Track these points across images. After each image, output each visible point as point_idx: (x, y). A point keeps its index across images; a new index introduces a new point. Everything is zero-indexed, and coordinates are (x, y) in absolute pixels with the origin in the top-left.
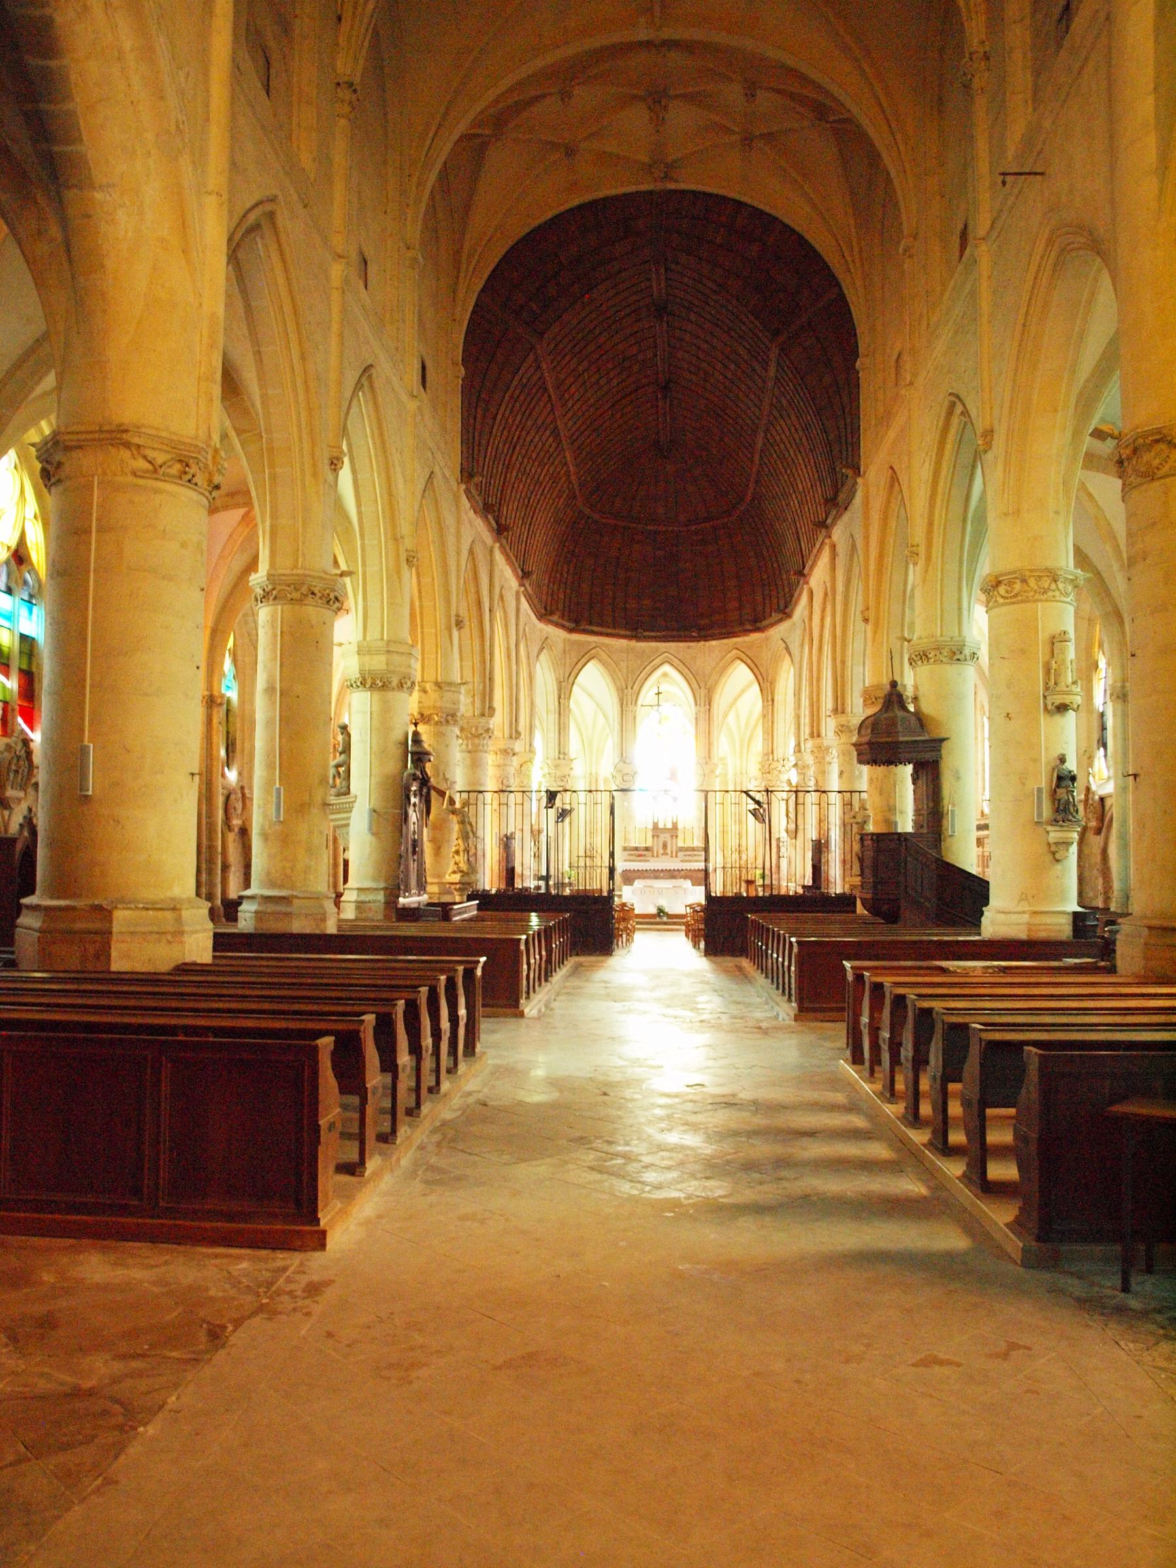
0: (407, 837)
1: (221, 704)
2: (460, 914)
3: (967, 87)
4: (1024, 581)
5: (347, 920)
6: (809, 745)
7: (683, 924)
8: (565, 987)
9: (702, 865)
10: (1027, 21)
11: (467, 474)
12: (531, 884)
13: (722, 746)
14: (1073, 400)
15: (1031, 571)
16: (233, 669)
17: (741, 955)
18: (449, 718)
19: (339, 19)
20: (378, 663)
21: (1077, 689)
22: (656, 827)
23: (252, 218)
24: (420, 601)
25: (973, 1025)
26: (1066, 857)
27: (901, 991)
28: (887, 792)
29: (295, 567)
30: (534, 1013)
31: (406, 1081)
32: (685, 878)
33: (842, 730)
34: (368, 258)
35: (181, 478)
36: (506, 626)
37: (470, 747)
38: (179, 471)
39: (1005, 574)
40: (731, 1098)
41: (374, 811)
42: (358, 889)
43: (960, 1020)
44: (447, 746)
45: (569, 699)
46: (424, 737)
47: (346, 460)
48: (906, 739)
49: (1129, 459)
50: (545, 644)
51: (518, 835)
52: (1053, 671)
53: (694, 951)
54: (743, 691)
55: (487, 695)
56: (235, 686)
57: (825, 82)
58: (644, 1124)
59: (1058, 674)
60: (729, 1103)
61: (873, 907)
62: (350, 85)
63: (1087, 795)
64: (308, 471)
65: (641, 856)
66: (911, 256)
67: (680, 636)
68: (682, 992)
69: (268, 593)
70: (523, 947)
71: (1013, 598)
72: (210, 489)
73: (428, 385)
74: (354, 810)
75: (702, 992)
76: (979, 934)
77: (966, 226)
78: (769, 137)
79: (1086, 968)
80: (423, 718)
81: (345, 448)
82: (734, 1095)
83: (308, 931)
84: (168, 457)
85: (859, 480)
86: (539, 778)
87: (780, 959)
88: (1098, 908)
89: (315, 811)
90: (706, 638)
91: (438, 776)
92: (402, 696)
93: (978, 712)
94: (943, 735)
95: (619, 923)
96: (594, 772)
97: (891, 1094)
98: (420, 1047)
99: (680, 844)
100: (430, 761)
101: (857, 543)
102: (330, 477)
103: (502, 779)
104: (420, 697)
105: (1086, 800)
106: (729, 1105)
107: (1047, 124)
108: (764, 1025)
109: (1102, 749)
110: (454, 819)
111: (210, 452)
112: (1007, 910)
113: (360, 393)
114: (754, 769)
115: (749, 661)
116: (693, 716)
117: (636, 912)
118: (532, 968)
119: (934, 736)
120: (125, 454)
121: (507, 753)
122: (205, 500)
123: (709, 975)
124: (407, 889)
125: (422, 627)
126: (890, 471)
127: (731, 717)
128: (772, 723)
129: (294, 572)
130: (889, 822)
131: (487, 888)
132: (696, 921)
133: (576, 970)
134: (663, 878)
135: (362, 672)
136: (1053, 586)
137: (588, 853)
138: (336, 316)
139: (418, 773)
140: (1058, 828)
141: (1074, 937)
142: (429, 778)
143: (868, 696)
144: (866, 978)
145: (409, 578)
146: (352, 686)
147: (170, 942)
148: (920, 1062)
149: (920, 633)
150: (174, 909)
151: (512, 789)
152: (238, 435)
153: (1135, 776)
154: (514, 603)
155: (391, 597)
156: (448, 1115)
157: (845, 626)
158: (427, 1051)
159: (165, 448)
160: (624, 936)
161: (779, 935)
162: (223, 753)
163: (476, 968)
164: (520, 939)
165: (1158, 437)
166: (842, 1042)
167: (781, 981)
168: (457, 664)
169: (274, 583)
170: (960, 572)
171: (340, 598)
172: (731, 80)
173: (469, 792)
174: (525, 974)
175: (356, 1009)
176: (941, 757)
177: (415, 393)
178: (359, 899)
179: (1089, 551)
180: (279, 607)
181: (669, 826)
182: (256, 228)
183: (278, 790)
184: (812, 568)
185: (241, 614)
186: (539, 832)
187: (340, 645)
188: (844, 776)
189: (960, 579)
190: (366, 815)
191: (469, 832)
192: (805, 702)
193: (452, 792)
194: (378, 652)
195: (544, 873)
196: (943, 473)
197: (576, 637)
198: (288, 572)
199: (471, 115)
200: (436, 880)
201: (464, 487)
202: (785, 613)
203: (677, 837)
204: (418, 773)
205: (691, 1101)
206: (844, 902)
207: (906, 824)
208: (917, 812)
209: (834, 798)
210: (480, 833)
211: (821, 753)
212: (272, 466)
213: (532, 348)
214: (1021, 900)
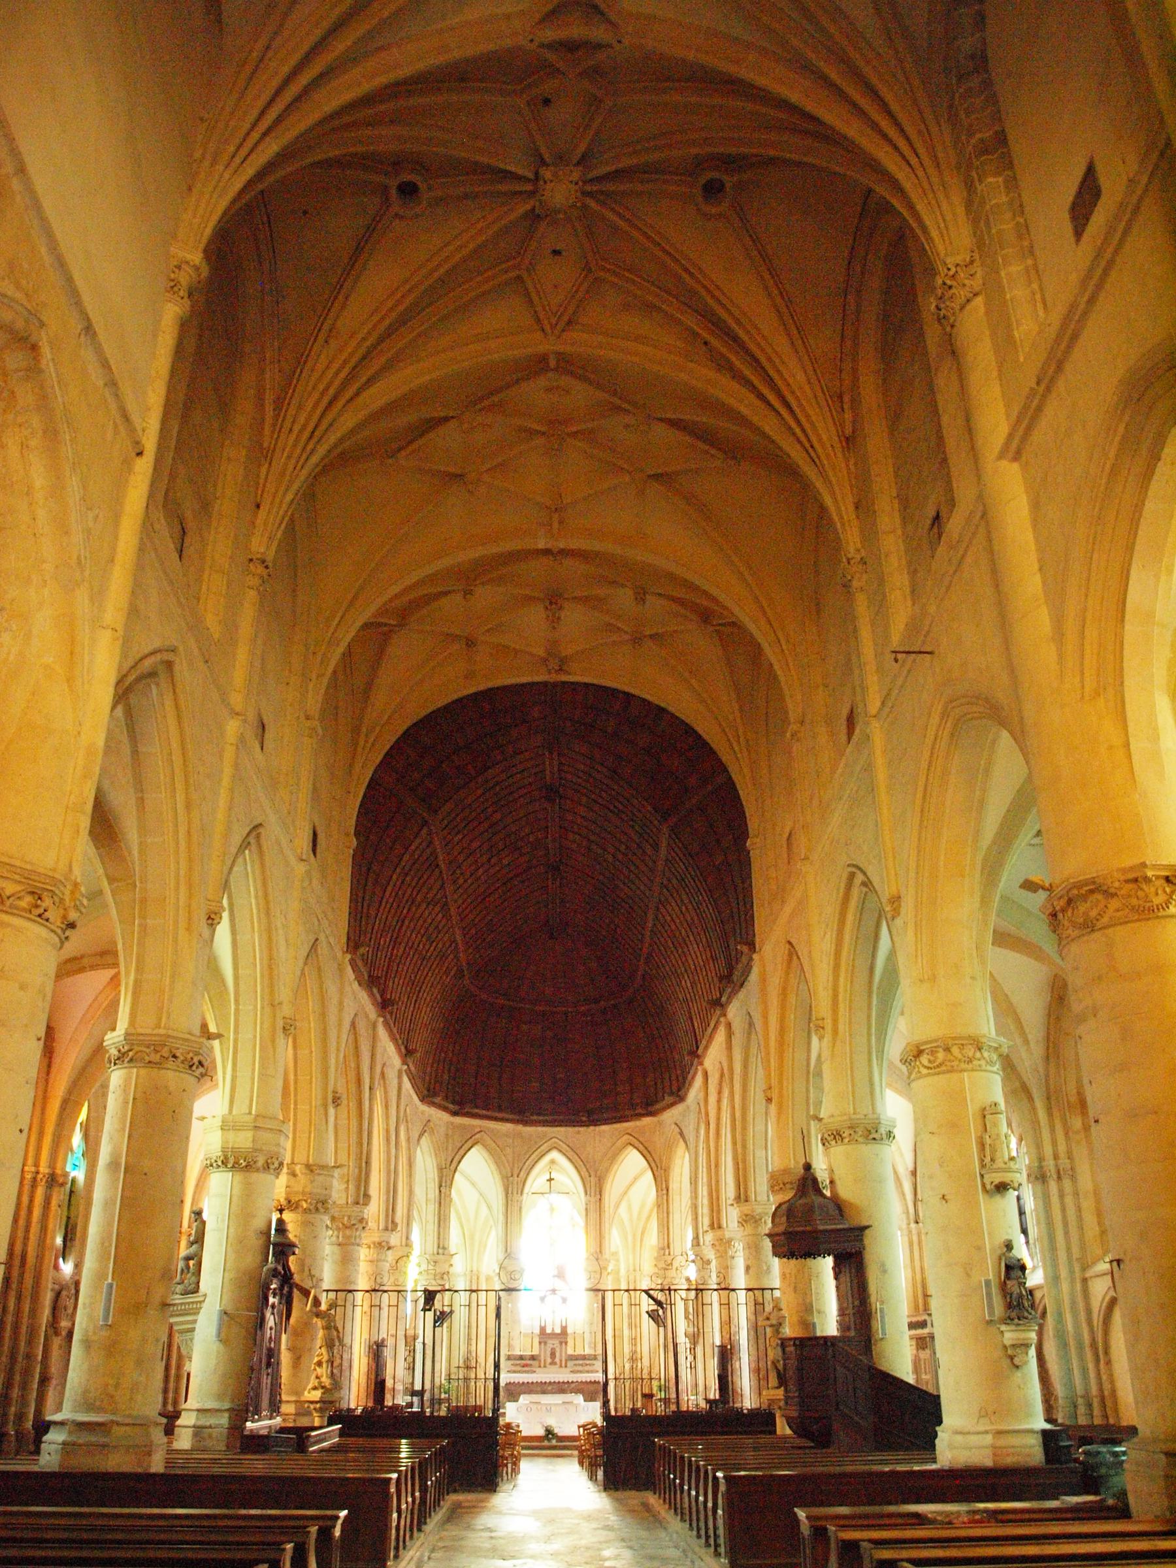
0: (261, 1346)
4: (947, 1049)
6: (709, 1238)
7: (576, 1448)
10: (899, 532)
11: (353, 944)
12: (401, 1400)
13: (615, 1239)
14: (979, 867)
15: (954, 1038)
16: (83, 1145)
18: (320, 1205)
19: (258, 506)
20: (244, 1140)
23: (148, 663)
24: (296, 1075)
26: (1026, 1363)
28: (803, 1290)
29: (158, 1026)
32: (577, 1391)
33: (748, 1219)
34: (265, 721)
36: (387, 1107)
38: (29, 904)
39: (926, 1043)
42: (198, 1410)
46: (290, 1227)
49: (1063, 911)
50: (427, 1127)
51: (390, 1342)
52: (987, 1147)
53: (590, 1484)
54: (635, 1179)
56: (83, 1165)
57: (715, 592)
59: (994, 1150)
61: (800, 1427)
62: (263, 562)
64: (182, 925)
65: (526, 1365)
68: (583, 1542)
69: (124, 1054)
70: (393, 1490)
71: (936, 1068)
72: (64, 926)
73: (318, 851)
76: (934, 1460)
77: (852, 712)
80: (291, 1204)
81: (225, 902)
84: (19, 888)
85: (755, 956)
86: (415, 1276)
87: (701, 1498)
90: (595, 1123)
91: (303, 1271)
94: (865, 1223)
95: (503, 1450)
96: (475, 1269)
99: (570, 1351)
100: (294, 1253)
101: (755, 1021)
102: (206, 932)
103: (376, 1275)
104: (288, 1181)
110: (319, 1323)
112: (966, 1430)
114: (648, 1265)
121: (382, 1246)
124: (257, 1411)
125: (296, 1104)
126: (787, 946)
127: (623, 1210)
128: (668, 1213)
129: (155, 1032)
130: (807, 1325)
131: (352, 1406)
136: (978, 1055)
138: (228, 771)
139: (280, 1268)
140: (1013, 1327)
141: (1049, 1460)
142: (292, 1275)
143: (776, 1183)
145: (285, 1050)
146: (211, 1165)
151: (385, 1288)
152: (109, 884)
154: (395, 1081)
155: (263, 1066)
159: (17, 877)
161: (698, 1467)
162: (59, 1241)
163: (334, 1527)
164: (390, 1479)
165: (1092, 887)
167: (702, 1524)
171: (205, 1064)
172: (623, 586)
173: (336, 1291)
174: (394, 1524)
178: (200, 1423)
181: (558, 1331)
182: (152, 674)
183: (111, 1286)
184: (706, 1048)
185: (98, 1084)
186: (415, 1338)
187: (202, 1119)
189: (870, 1053)
190: (215, 1318)
191: (335, 1341)
192: (703, 1191)
195: (418, 1387)
197: (459, 1120)
198: (149, 1031)
199: (380, 601)
200: (293, 1398)
201: (349, 956)
202: (678, 1096)
203: (566, 1343)
204: (280, 1268)
206: (761, 1420)
207: (829, 1325)
208: (842, 1312)
210: (347, 1340)
211: (722, 1246)
213: (426, 823)
214: (980, 1417)
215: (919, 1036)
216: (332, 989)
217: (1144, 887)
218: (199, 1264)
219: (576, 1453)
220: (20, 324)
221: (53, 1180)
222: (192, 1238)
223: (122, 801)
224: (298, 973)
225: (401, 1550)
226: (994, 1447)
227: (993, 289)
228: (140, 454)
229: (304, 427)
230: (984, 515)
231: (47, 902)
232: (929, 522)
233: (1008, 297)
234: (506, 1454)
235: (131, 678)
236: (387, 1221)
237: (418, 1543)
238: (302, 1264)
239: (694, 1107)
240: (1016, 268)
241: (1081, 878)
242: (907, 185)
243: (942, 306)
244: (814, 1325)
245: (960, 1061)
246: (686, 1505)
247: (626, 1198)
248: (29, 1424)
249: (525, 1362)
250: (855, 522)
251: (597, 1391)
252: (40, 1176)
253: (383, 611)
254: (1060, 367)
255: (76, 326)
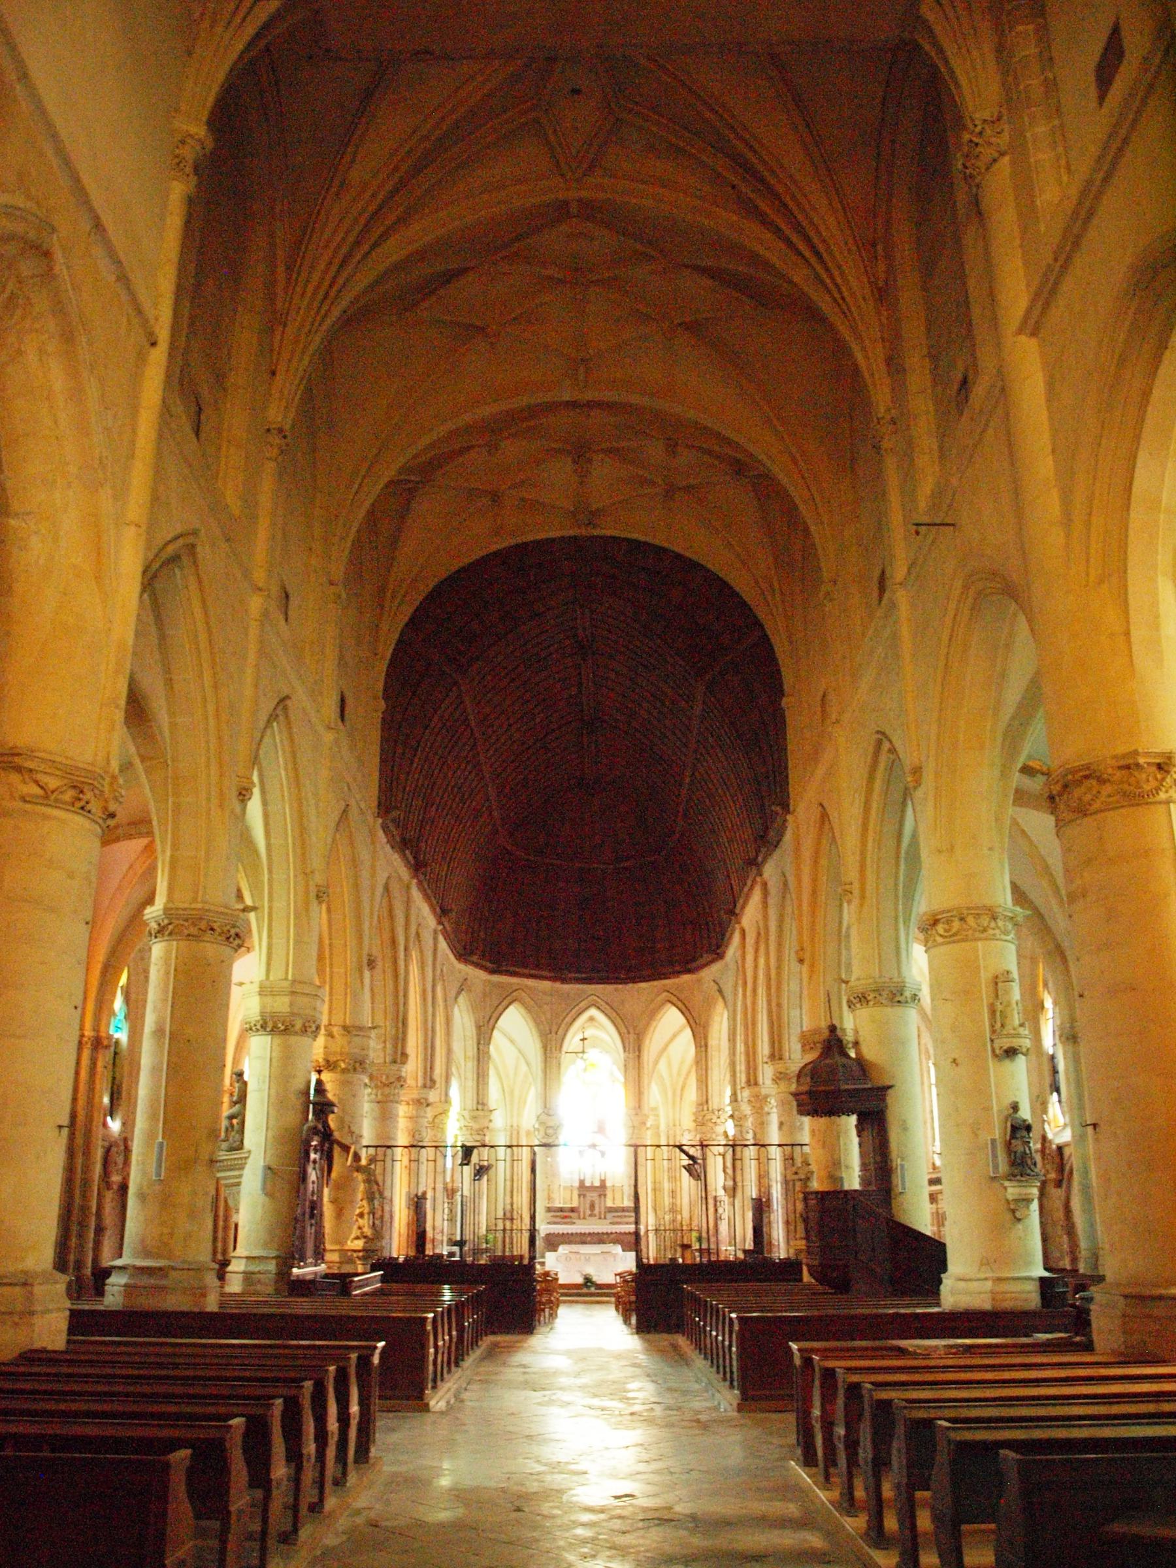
1: (107, 1047)
2: (360, 1287)
3: (877, 448)
4: (962, 919)
5: (231, 1295)
6: (745, 1094)
7: (614, 1295)
8: (477, 1374)
9: (631, 1228)
11: (385, 807)
13: (654, 1095)
15: (968, 908)
16: (124, 1008)
17: (677, 1332)
19: (274, 373)
20: (282, 1005)
21: (1025, 1031)
22: (582, 1182)
23: (170, 549)
25: (940, 1422)
27: (855, 1378)
28: (831, 1144)
29: (195, 900)
30: (442, 1405)
31: (280, 1498)
32: (615, 1242)
33: (779, 1077)
34: (291, 592)
35: (73, 805)
37: (380, 1097)
39: (943, 912)
40: (666, 1512)
41: (270, 1168)
42: (247, 1258)
43: (922, 1414)
44: (354, 1096)
45: (489, 1044)
46: (329, 1086)
47: (256, 791)
48: (846, 1087)
49: (1060, 794)
51: (429, 1195)
52: (998, 1014)
53: (624, 1328)
54: (675, 1036)
55: (400, 1040)
56: (125, 1027)
58: (564, 1549)
59: (1004, 1015)
60: (661, 1519)
61: (820, 1274)
62: (280, 430)
63: (1043, 1145)
64: (215, 801)
65: (566, 1217)
66: (831, 600)
67: (608, 978)
68: (610, 1377)
70: (429, 1328)
71: (952, 938)
73: (347, 717)
74: (247, 1166)
75: (634, 1377)
76: (938, 1305)
77: (883, 572)
78: (688, 489)
79: (1059, 1345)
80: (330, 1065)
81: (255, 778)
82: (670, 1508)
83: (185, 1308)
85: (788, 817)
86: (455, 1131)
87: (720, 1338)
88: (1064, 1270)
89: (200, 1168)
90: (634, 980)
92: (306, 1040)
93: (923, 1056)
97: (849, 1504)
98: (301, 1456)
99: (609, 1204)
103: (414, 1133)
104: (326, 1041)
105: (1043, 1151)
106: (663, 1521)
107: (954, 481)
108: (703, 1417)
109: (1055, 1094)
110: (360, 1177)
111: (108, 780)
113: (275, 724)
114: (688, 1122)
115: (679, 1004)
116: (622, 1063)
117: (561, 1281)
118: (440, 1352)
119: (880, 1084)
120: (15, 778)
121: (421, 1103)
122: (97, 826)
123: (641, 1356)
124: (303, 1258)
127: (662, 1065)
129: (193, 906)
130: (835, 1179)
132: (628, 1293)
133: (492, 1353)
134: (590, 1243)
135: (262, 1014)
136: (993, 924)
137: (508, 1215)
138: (253, 648)
139: (320, 1126)
140: (1015, 1184)
141: (1043, 1306)
143: (806, 1043)
144: (815, 1363)
145: (319, 914)
147: (17, 1324)
148: (880, 1464)
149: (860, 973)
150: (25, 1284)
152: (142, 761)
153: (1095, 1126)
154: (431, 942)
156: (331, 1541)
157: (779, 968)
158: (308, 1461)
160: (547, 1310)
162: (106, 1100)
163: (372, 1355)
165: (1087, 772)
166: (792, 1439)
168: (367, 1005)
169: (170, 919)
170: (896, 909)
173: (377, 1147)
174: (431, 1358)
175: (223, 1410)
176: (886, 1106)
177: (333, 725)
179: (1025, 886)
180: (175, 943)
181: (597, 1184)
182: (175, 559)
183: (161, 1144)
184: (743, 907)
187: (241, 984)
188: (784, 1128)
189: (896, 918)
191: (376, 1193)
192: (740, 1048)
193: (358, 1146)
194: (279, 993)
195: (458, 1238)
196: (874, 805)
197: (496, 978)
198: (186, 906)
199: (402, 460)
200: (337, 1247)
201: (380, 821)
204: (320, 1126)
205: (620, 1517)
206: (789, 1269)
207: (853, 1181)
208: (864, 1167)
209: (775, 1153)
210: (387, 1194)
211: (759, 1102)
212: (176, 794)
214: (982, 1265)
215: (936, 906)
216: (364, 854)
217: (1136, 773)
218: (242, 1124)
219: (613, 1299)
220: (32, 235)
221: (98, 1043)
222: (235, 1099)
223: (152, 684)
224: (329, 840)
225: (439, 1383)
226: (992, 1292)
227: (1018, 149)
228: (154, 344)
229: (318, 287)
230: (1003, 389)
231: (89, 795)
232: (956, 387)
233: (1032, 160)
234: (544, 1300)
235: (155, 566)
236: (425, 1078)
237: (457, 1376)
238: (341, 1121)
239: (732, 966)
240: (1041, 129)
241: (1076, 764)
242: (937, 29)
243: (968, 164)
244: (841, 1179)
245: (975, 930)
246: (709, 1346)
247: (665, 1054)
248: (88, 1271)
249: (564, 1214)
250: (888, 381)
251: (634, 1242)
252: (85, 1039)
253: (403, 470)
254: (1076, 244)
255: (86, 226)
